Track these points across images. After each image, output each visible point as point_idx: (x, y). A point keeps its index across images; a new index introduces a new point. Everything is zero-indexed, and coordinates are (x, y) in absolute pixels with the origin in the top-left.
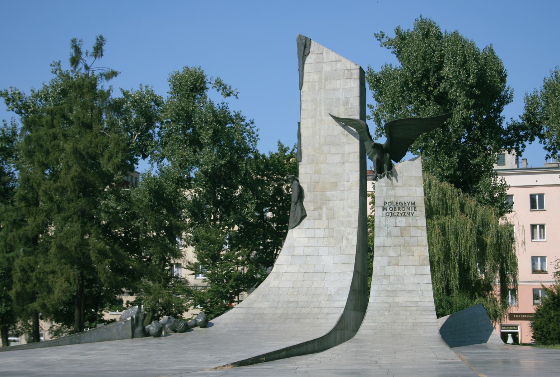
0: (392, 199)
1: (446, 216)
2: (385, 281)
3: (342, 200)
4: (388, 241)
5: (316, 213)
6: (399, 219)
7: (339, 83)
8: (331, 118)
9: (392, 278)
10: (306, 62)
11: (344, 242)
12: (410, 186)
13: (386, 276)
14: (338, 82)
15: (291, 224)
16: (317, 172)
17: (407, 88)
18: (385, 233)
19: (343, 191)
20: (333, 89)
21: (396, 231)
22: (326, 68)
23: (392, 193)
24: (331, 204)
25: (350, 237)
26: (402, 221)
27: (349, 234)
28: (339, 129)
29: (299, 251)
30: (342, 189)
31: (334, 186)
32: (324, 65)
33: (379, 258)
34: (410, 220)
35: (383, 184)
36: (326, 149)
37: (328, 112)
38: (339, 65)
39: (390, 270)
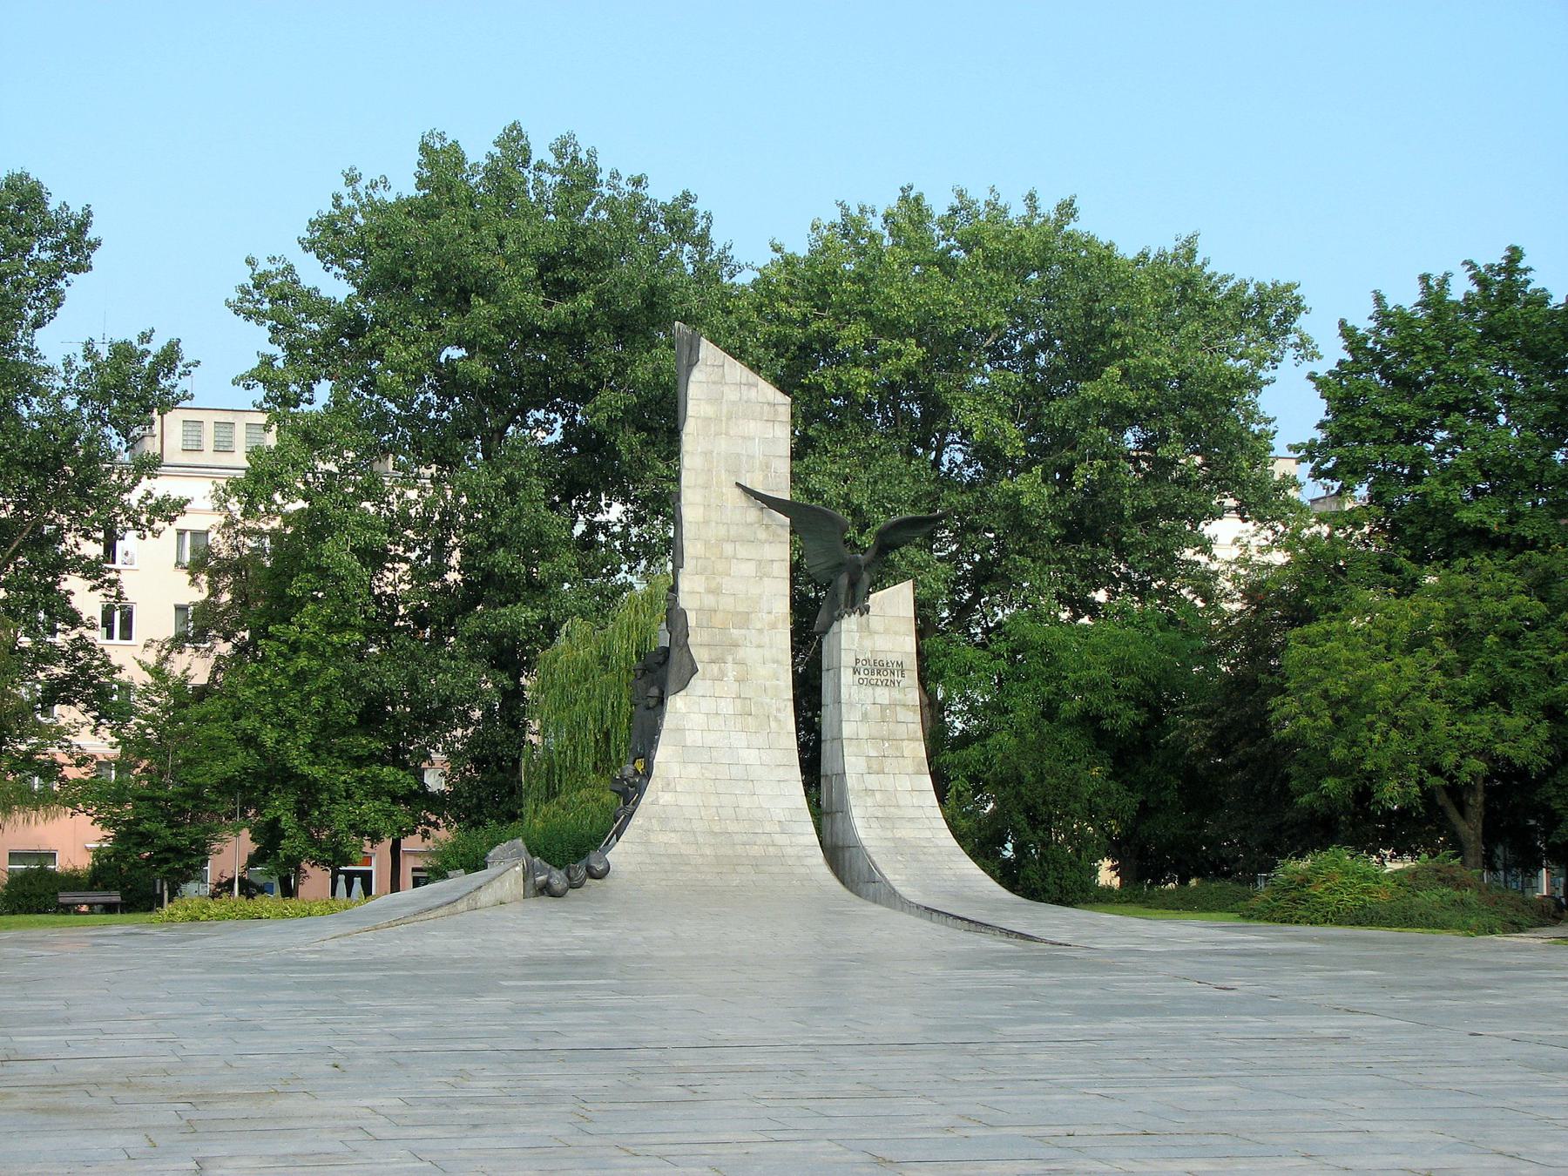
0: (869, 655)
1: (474, 760)
2: (870, 801)
3: (759, 646)
4: (864, 731)
5: (715, 667)
6: (879, 690)
7: (752, 427)
8: (738, 491)
9: (878, 795)
10: (692, 378)
11: (773, 724)
12: (896, 633)
13: (868, 791)
14: (752, 424)
15: (671, 686)
16: (716, 591)
17: (1052, 371)
18: (858, 716)
19: (761, 631)
20: (744, 438)
21: (875, 712)
22: (731, 394)
23: (868, 643)
24: (741, 653)
25: (781, 716)
26: (883, 695)
27: (779, 710)
28: (753, 513)
29: (692, 738)
30: (759, 626)
31: (744, 620)
32: (726, 389)
33: (853, 759)
34: (896, 694)
35: (855, 627)
36: (728, 549)
37: (734, 479)
38: (753, 393)
39: (872, 781)
